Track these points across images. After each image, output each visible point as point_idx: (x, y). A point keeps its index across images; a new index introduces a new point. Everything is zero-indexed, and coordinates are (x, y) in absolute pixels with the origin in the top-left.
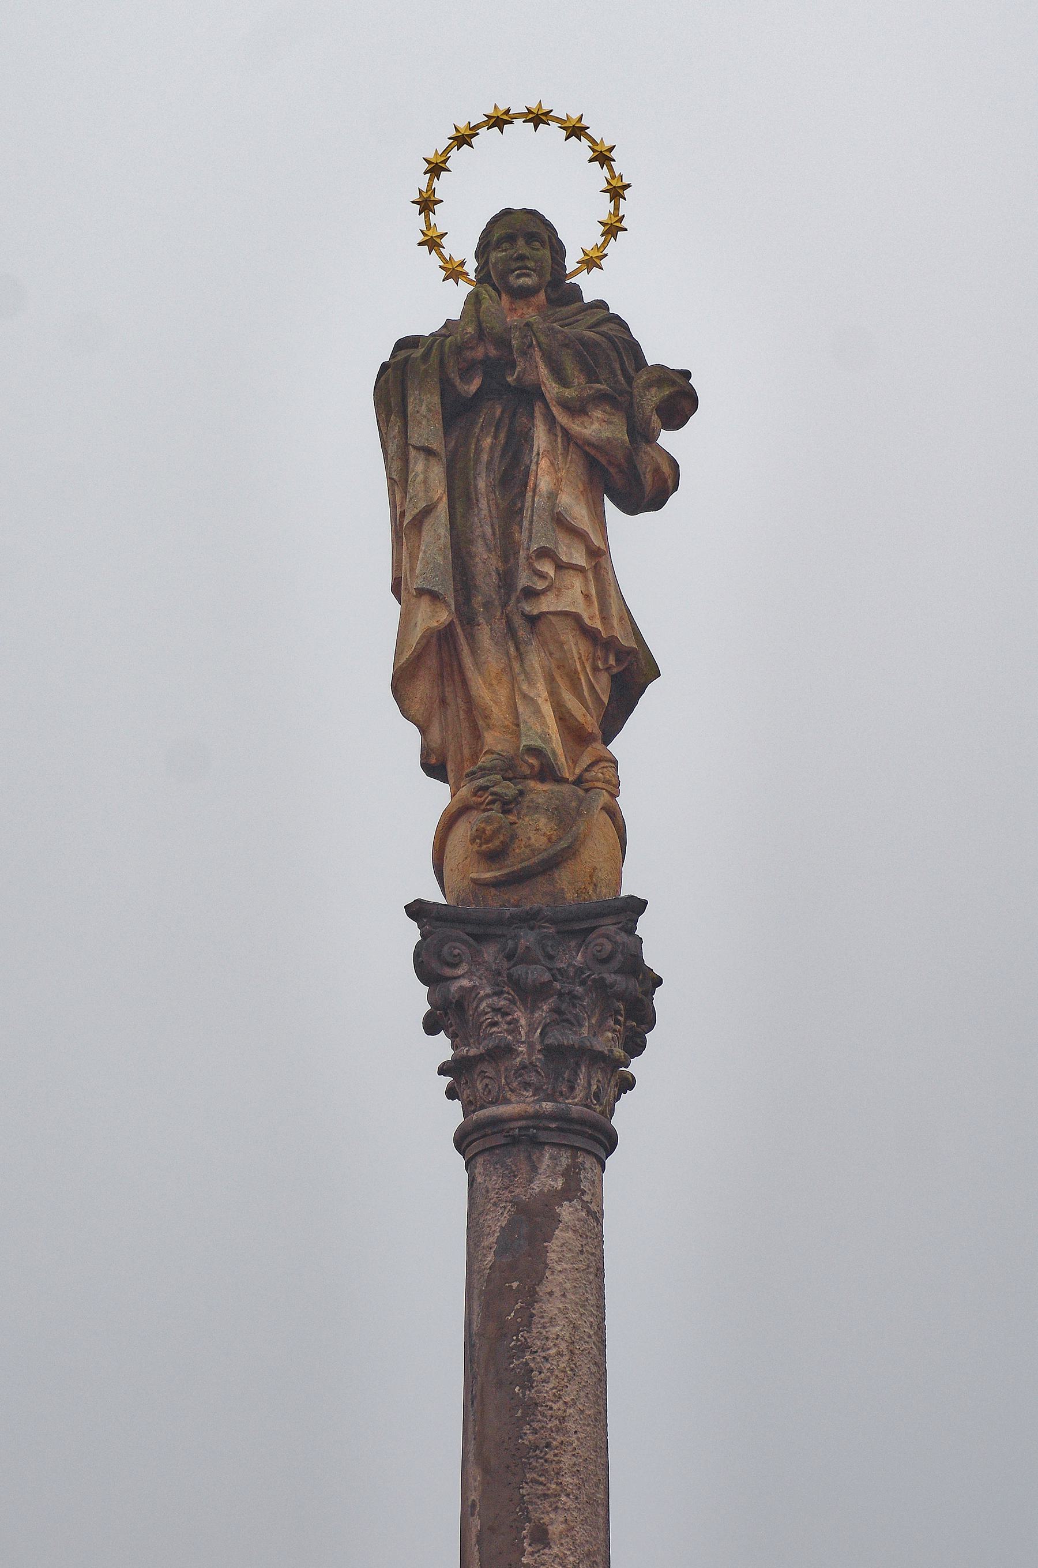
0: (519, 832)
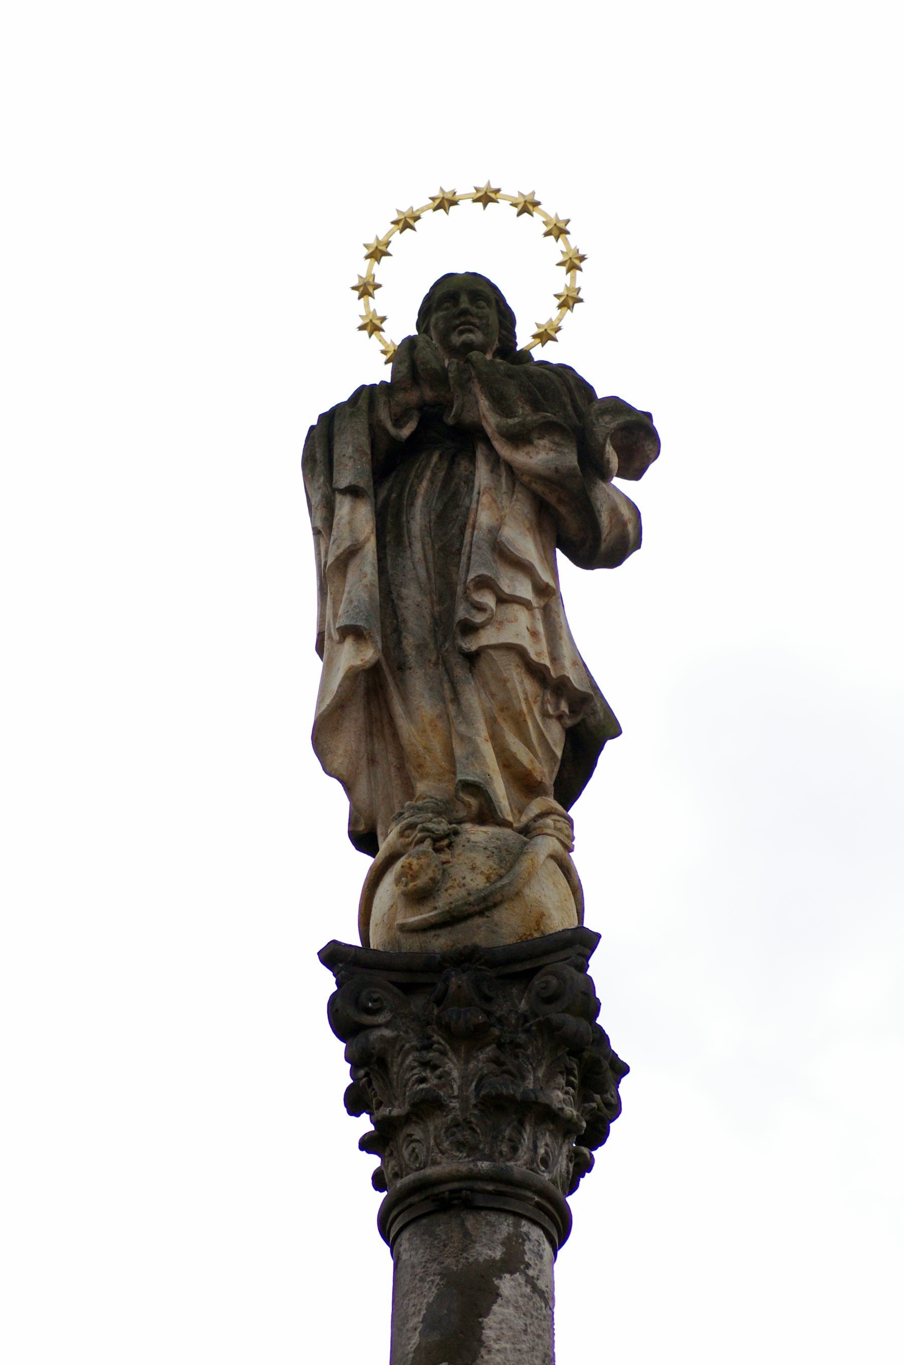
0: (453, 871)
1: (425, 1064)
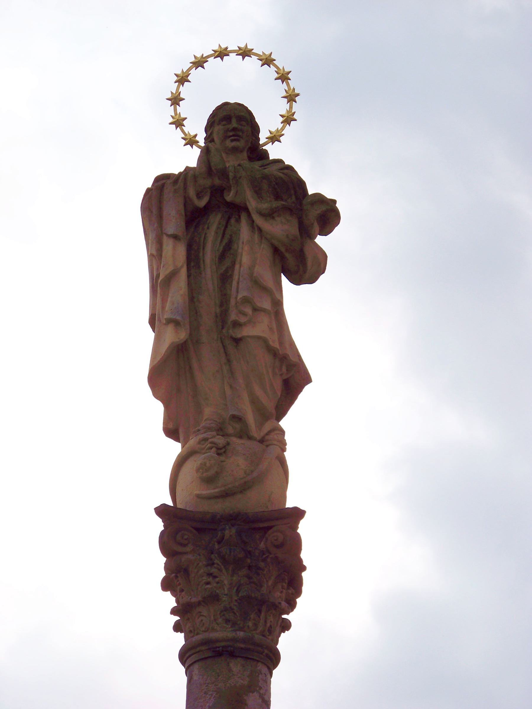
1: (210, 575)
